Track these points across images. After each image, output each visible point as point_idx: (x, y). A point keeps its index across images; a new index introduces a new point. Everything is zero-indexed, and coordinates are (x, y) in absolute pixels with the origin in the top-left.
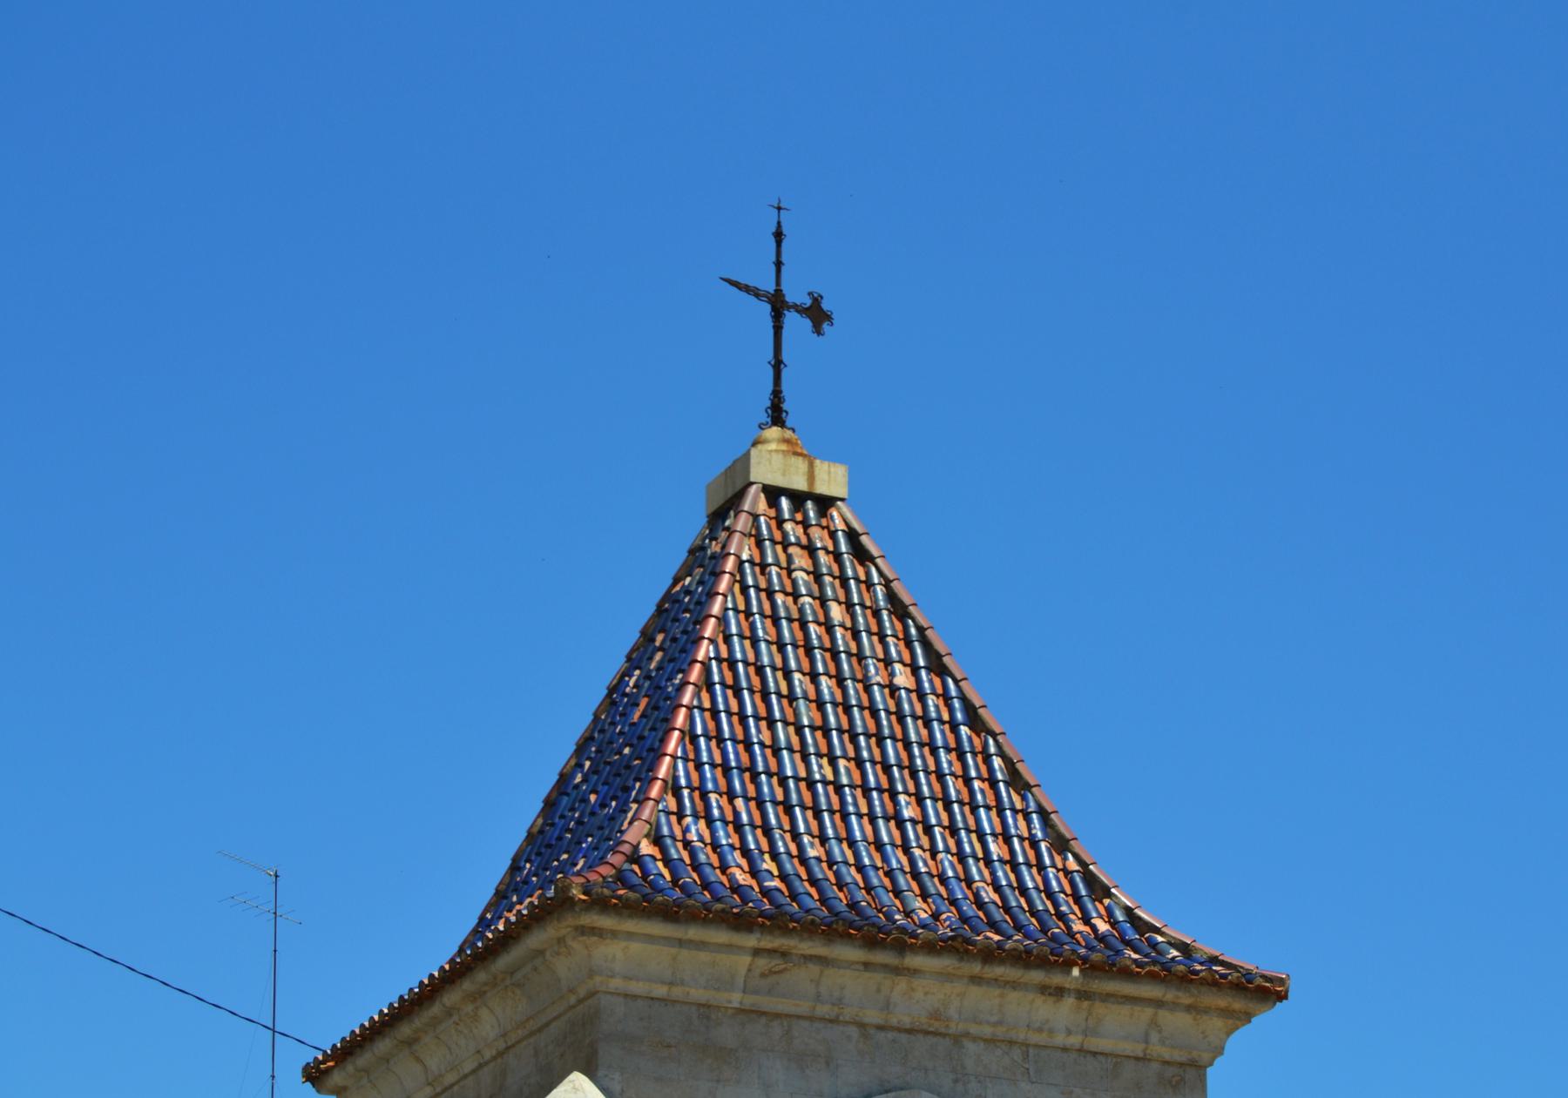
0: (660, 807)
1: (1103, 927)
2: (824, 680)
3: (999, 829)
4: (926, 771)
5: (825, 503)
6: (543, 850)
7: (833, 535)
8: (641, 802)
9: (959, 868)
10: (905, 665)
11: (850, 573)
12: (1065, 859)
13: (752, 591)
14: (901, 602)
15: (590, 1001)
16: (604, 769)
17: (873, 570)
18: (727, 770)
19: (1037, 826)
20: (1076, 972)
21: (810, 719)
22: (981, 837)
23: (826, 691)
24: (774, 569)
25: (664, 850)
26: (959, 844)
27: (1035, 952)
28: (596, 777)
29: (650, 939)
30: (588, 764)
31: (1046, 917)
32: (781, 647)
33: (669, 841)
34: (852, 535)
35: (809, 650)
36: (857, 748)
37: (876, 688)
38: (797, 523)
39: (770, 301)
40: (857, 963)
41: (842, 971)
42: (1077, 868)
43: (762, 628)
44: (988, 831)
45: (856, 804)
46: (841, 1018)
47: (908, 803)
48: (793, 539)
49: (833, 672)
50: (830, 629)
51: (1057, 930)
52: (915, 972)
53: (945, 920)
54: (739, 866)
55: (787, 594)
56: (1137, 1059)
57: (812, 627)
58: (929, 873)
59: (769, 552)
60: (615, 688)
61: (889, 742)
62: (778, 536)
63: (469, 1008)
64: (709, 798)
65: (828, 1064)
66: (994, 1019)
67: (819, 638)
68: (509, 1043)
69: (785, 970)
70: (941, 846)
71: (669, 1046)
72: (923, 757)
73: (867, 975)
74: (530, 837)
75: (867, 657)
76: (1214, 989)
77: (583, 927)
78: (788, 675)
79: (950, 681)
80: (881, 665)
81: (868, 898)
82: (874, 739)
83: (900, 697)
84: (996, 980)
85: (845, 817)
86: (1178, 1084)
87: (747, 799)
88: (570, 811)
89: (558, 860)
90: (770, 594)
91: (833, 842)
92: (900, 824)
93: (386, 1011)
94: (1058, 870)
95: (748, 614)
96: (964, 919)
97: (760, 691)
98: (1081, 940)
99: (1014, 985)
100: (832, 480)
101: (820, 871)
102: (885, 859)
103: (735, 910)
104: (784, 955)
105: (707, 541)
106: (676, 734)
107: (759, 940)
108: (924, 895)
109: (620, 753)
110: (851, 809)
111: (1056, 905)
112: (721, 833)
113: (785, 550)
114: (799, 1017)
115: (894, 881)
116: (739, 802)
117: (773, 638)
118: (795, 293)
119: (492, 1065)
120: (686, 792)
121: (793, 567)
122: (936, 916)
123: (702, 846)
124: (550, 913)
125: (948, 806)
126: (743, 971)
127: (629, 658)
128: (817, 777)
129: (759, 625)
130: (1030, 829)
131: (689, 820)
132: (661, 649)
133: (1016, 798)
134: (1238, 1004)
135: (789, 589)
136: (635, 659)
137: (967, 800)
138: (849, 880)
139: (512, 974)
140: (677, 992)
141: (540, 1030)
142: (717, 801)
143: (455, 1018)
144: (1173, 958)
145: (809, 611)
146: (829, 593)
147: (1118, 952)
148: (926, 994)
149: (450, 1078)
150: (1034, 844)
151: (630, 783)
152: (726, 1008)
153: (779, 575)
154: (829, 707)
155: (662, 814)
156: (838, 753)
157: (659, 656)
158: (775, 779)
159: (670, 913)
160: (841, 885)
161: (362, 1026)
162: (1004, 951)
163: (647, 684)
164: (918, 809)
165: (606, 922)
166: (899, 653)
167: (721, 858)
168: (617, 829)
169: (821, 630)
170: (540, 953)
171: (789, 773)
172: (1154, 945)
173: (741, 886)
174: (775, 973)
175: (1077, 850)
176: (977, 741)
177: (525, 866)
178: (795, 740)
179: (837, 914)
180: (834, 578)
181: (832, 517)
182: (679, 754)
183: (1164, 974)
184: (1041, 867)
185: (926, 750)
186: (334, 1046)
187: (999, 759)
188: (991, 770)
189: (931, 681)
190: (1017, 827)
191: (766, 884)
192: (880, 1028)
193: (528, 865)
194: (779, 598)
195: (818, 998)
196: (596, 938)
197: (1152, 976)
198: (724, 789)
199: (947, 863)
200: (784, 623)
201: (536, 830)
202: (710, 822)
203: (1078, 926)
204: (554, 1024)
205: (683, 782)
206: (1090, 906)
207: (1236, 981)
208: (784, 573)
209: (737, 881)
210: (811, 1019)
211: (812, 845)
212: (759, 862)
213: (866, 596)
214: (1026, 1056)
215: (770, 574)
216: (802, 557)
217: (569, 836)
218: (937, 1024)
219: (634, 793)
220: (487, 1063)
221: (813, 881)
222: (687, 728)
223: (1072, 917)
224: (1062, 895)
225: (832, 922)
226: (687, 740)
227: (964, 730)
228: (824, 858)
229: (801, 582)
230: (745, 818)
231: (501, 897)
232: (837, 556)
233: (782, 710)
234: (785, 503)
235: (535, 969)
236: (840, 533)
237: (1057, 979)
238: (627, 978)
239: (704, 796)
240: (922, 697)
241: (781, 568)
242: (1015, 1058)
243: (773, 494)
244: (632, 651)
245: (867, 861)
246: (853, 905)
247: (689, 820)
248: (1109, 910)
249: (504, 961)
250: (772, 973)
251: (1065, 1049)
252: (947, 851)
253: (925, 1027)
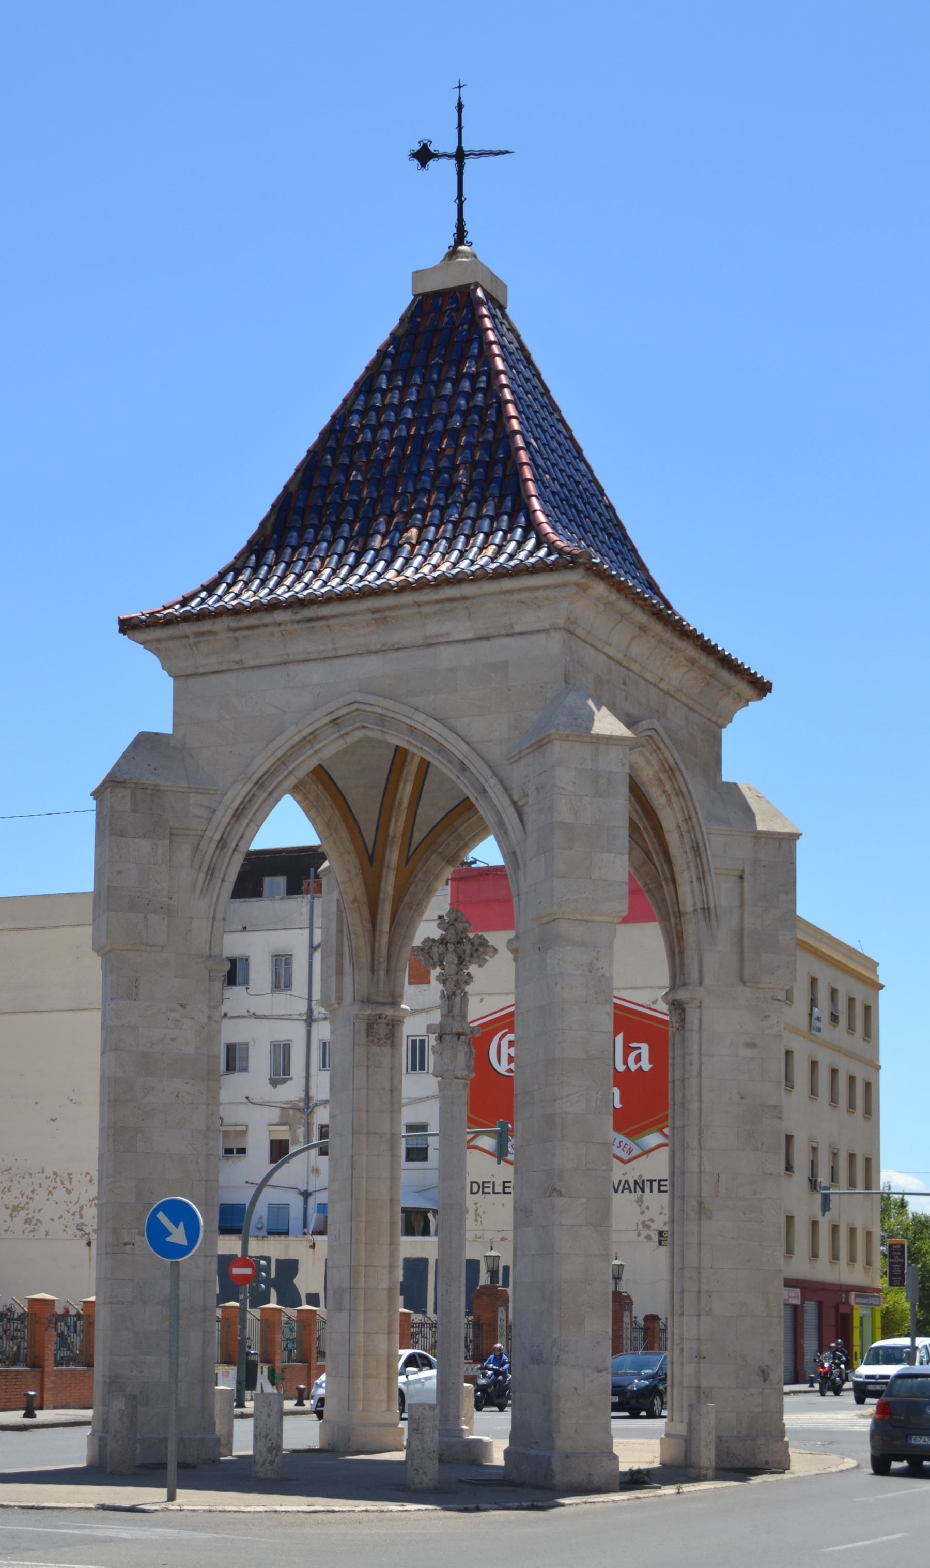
149: (635, 667)
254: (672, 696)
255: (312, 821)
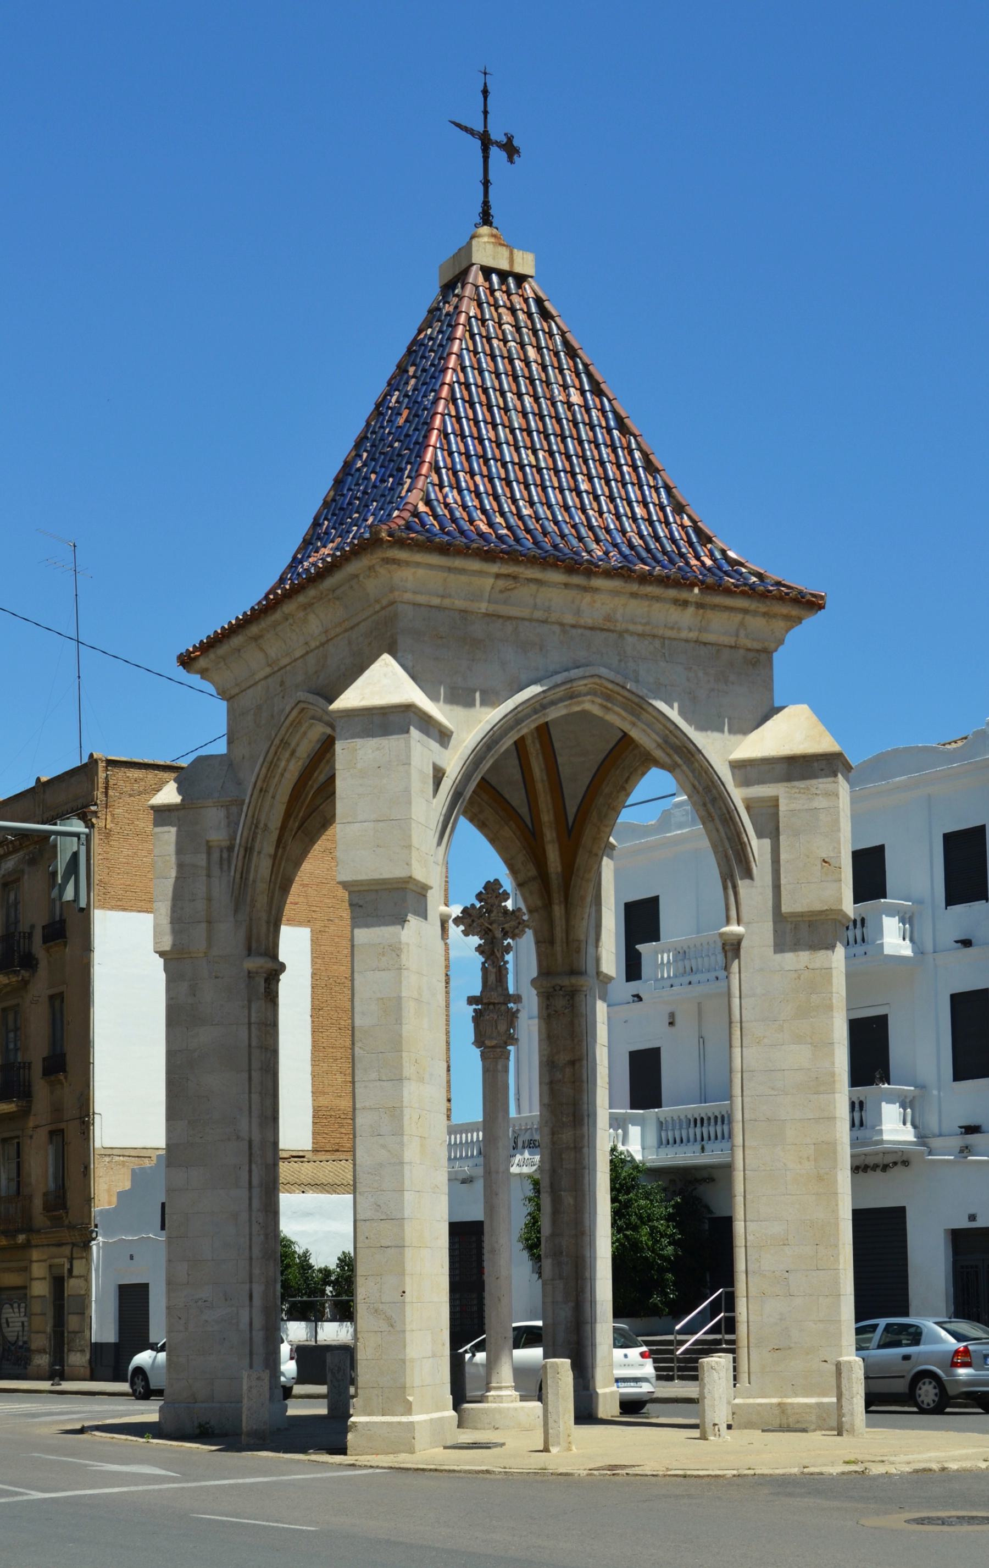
0: (428, 481)
1: (709, 562)
2: (526, 398)
3: (640, 499)
4: (593, 459)
5: (521, 279)
6: (337, 512)
7: (526, 301)
8: (415, 476)
9: (617, 523)
10: (577, 389)
11: (539, 326)
12: (682, 518)
13: (477, 337)
14: (573, 347)
15: (390, 608)
16: (379, 457)
17: (553, 324)
18: (468, 457)
19: (664, 496)
20: (696, 590)
21: (519, 423)
22: (630, 503)
23: (528, 405)
24: (490, 323)
25: (432, 509)
26: (616, 507)
27: (672, 577)
28: (374, 463)
29: (430, 567)
30: (365, 455)
31: (673, 555)
32: (498, 376)
33: (435, 503)
34: (539, 301)
35: (515, 378)
36: (549, 444)
37: (559, 404)
38: (504, 292)
39: (480, 139)
40: (560, 584)
41: (551, 589)
42: (690, 524)
43: (485, 363)
44: (634, 500)
45: (551, 481)
46: (549, 620)
47: (583, 481)
48: (501, 303)
49: (532, 393)
50: (528, 364)
51: (681, 564)
52: (596, 590)
53: (613, 557)
54: (481, 520)
55: (500, 340)
56: (731, 647)
57: (517, 362)
58: (599, 526)
59: (487, 311)
60: (380, 406)
61: (569, 439)
62: (491, 301)
63: (301, 614)
64: (458, 476)
65: (541, 650)
66: (644, 621)
67: (522, 369)
68: (329, 637)
69: (515, 588)
70: (605, 509)
71: (441, 638)
72: (591, 450)
73: (566, 591)
74: (326, 504)
75: (552, 384)
76: (781, 602)
77: (387, 558)
78: (503, 394)
79: (605, 400)
80: (561, 389)
81: (563, 542)
82: (559, 438)
83: (574, 410)
84: (646, 595)
85: (544, 489)
86: (755, 664)
87: (482, 476)
88: (355, 485)
89: (351, 518)
90: (489, 339)
91: (538, 505)
92: (579, 494)
93: (241, 617)
94: (679, 525)
95: (476, 353)
96: (625, 557)
97: (486, 405)
98: (696, 570)
99: (657, 599)
100: (525, 263)
101: (532, 524)
102: (571, 517)
103: (485, 548)
104: (515, 578)
105: (441, 304)
106: (435, 432)
107: (500, 568)
108: (597, 541)
109: (391, 446)
110: (548, 484)
111: (678, 548)
112: (468, 498)
113: (496, 310)
114: (523, 619)
115: (578, 531)
116: (478, 478)
117: (492, 369)
118: (497, 134)
119: (316, 651)
120: (444, 471)
121: (502, 322)
122: (606, 553)
123: (457, 506)
124: (365, 549)
125: (608, 482)
126: (488, 588)
127: (389, 384)
128: (526, 462)
129: (483, 360)
130: (659, 498)
131: (447, 489)
132: (414, 376)
133: (650, 478)
134: (795, 612)
135: (501, 337)
136: (395, 382)
137: (619, 479)
138: (550, 530)
139: (334, 591)
140: (447, 602)
141: (352, 628)
142: (464, 477)
143: (291, 621)
144: (754, 582)
145: (514, 352)
146: (527, 340)
147: (721, 578)
148: (603, 604)
149: (285, 661)
150: (662, 508)
151: (403, 465)
152: (477, 613)
153: (494, 327)
154: (530, 416)
155: (429, 485)
156: (538, 446)
157: (413, 381)
158: (499, 464)
159: (444, 550)
160: (545, 533)
161: (223, 628)
162: (653, 576)
163: (406, 400)
164: (589, 484)
165: (402, 555)
166: (572, 380)
167: (469, 514)
168: (396, 496)
169: (522, 365)
170: (356, 576)
171: (508, 459)
172: (741, 574)
173: (484, 533)
174: (509, 590)
175: (690, 512)
176: (623, 440)
177: (323, 524)
178: (510, 438)
179: (547, 552)
180: (529, 330)
181: (525, 289)
182: (438, 446)
183: (751, 592)
184: (667, 523)
185: (592, 445)
186: (202, 641)
187: (639, 452)
188: (633, 459)
189: (593, 400)
190: (651, 497)
191: (500, 532)
192: (573, 626)
193: (326, 523)
194: (495, 342)
195: (535, 607)
196: (396, 566)
197: (743, 593)
198: (468, 470)
199: (609, 520)
200: (499, 359)
201: (329, 499)
202: (460, 491)
203: (693, 562)
204: (363, 624)
205: (441, 464)
206: (699, 548)
207: (794, 597)
208: (497, 325)
209: (481, 530)
210: (530, 620)
211: (526, 508)
212: (493, 517)
213: (549, 342)
214: (663, 645)
215: (488, 326)
216: (507, 315)
217: (358, 502)
218: (608, 624)
219: (407, 472)
220: (312, 651)
221: (528, 531)
222: (442, 429)
223: (689, 555)
224: (682, 542)
225: (546, 557)
226: (442, 436)
227: (616, 433)
228: (533, 516)
229: (508, 331)
230: (482, 489)
231: (308, 544)
232: (530, 315)
233: (501, 417)
234: (495, 278)
235: (351, 587)
236: (531, 299)
237: (684, 595)
238: (415, 593)
239: (455, 473)
240: (588, 410)
241: (495, 323)
242: (657, 646)
243: (487, 272)
244: (392, 378)
245: (560, 518)
246: (555, 546)
247: (447, 489)
248: (711, 551)
249: (330, 582)
250: (507, 590)
251: (687, 641)
252: (609, 512)
253: (601, 626)
254: (328, 641)
255: (493, 841)
